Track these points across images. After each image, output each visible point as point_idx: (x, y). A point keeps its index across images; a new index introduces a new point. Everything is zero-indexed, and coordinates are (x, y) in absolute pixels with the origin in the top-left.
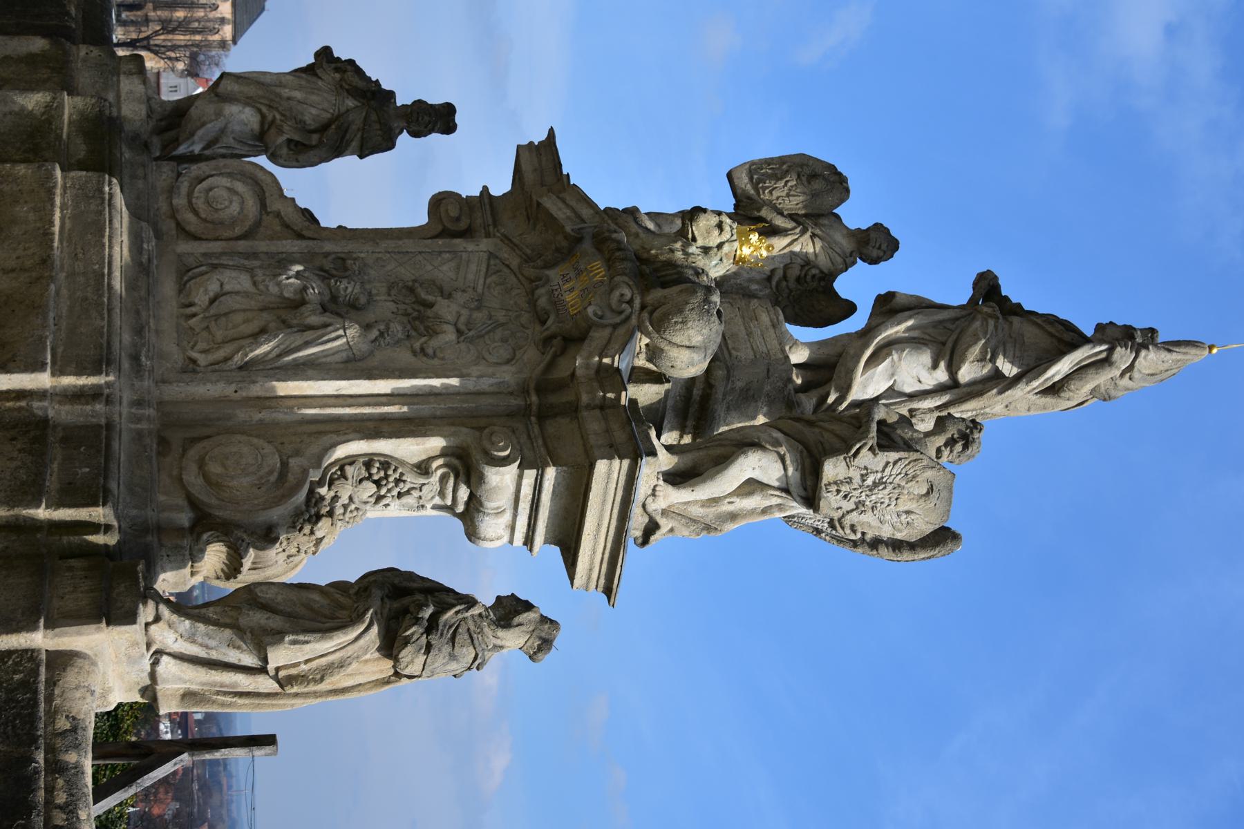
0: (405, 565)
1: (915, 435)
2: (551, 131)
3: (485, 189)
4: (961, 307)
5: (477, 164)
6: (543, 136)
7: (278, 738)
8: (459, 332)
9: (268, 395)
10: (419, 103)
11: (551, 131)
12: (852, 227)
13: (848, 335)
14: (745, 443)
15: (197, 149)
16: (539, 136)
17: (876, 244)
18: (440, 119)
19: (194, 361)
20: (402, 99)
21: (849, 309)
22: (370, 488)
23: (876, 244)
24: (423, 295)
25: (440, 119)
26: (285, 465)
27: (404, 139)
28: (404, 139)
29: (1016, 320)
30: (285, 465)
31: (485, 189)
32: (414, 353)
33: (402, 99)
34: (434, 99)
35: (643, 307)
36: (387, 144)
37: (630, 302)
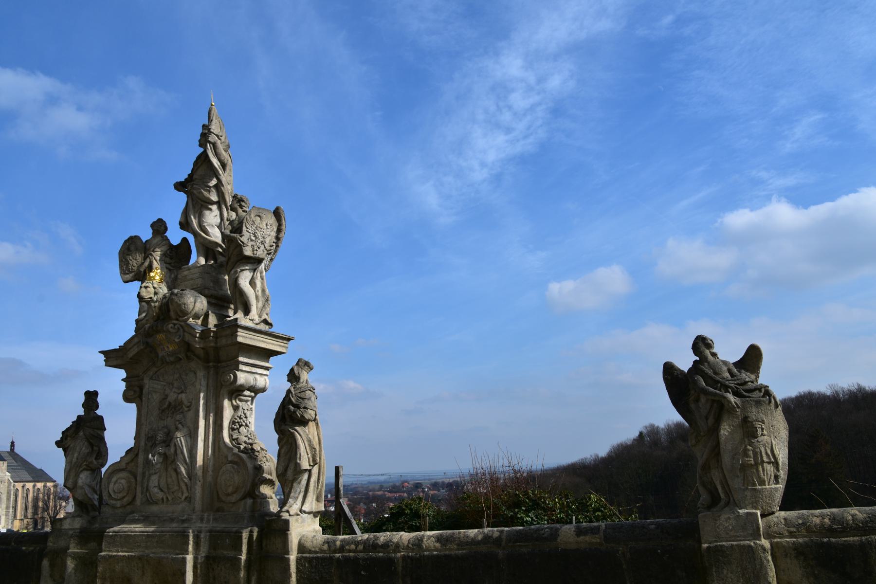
5: (112, 383)
6: (102, 356)
8: (182, 392)
10: (84, 405)
14: (235, 284)
15: (96, 497)
17: (159, 227)
18: (91, 398)
19: (186, 498)
21: (185, 240)
23: (159, 227)
25: (91, 398)
26: (231, 462)
27: (99, 412)
28: (99, 412)
29: (195, 177)
30: (231, 462)
35: (177, 320)
36: (101, 419)
37: (175, 325)
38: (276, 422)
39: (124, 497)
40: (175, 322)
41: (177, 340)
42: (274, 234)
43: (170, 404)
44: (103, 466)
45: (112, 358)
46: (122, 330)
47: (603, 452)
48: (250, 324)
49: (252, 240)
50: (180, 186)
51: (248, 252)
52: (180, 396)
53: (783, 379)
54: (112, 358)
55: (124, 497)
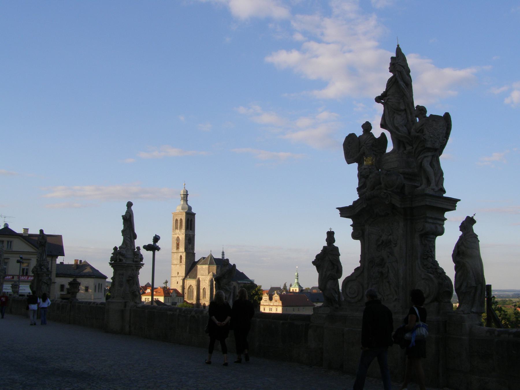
0: (451, 252)
1: (397, 75)
2: (337, 208)
3: (351, 225)
4: (384, 107)
5: (344, 228)
6: (338, 210)
7: (63, 284)
8: (390, 235)
9: (190, 274)
10: (327, 240)
11: (337, 208)
12: (362, 133)
13: (391, 136)
14: (421, 166)
15: (337, 296)
16: (338, 211)
17: (367, 127)
18: (331, 235)
19: (396, 299)
20: (325, 244)
21: (383, 135)
22: (429, 258)
23: (367, 127)
24: (380, 243)
25: (331, 235)
26: (423, 279)
27: (335, 244)
28: (335, 244)
29: (388, 93)
30: (423, 279)
31: (351, 225)
32: (396, 246)
33: (325, 244)
34: (326, 237)
35: (386, 190)
36: (337, 249)
37: (385, 193)
38: (453, 256)
39: (356, 297)
40: (385, 191)
41: (387, 203)
42: (445, 132)
43: (383, 241)
44: (340, 277)
45: (344, 212)
46: (350, 196)
47: (348, 206)
48: (431, 192)
49: (431, 137)
50: (378, 100)
51: (429, 145)
52: (389, 237)
53: (118, 247)
54: (344, 212)
55: (356, 297)
